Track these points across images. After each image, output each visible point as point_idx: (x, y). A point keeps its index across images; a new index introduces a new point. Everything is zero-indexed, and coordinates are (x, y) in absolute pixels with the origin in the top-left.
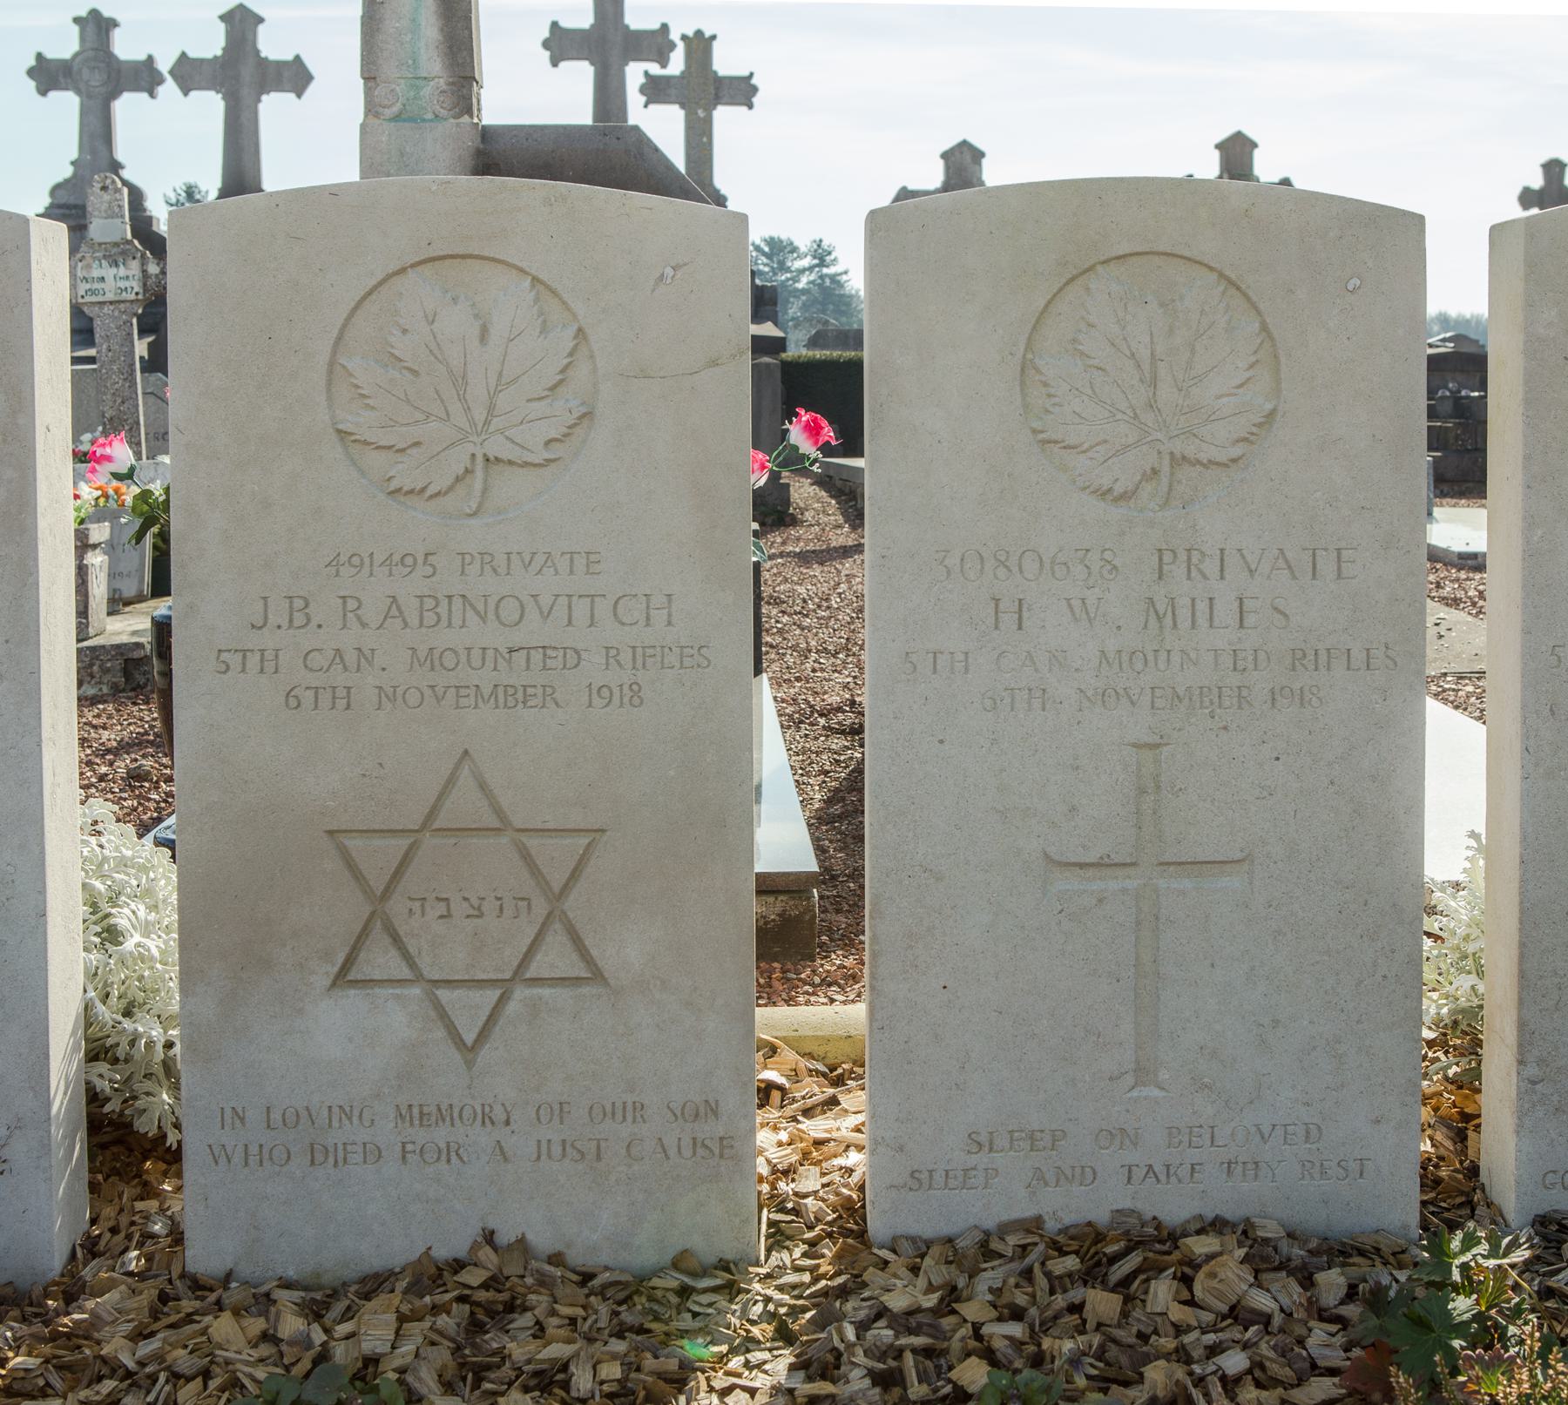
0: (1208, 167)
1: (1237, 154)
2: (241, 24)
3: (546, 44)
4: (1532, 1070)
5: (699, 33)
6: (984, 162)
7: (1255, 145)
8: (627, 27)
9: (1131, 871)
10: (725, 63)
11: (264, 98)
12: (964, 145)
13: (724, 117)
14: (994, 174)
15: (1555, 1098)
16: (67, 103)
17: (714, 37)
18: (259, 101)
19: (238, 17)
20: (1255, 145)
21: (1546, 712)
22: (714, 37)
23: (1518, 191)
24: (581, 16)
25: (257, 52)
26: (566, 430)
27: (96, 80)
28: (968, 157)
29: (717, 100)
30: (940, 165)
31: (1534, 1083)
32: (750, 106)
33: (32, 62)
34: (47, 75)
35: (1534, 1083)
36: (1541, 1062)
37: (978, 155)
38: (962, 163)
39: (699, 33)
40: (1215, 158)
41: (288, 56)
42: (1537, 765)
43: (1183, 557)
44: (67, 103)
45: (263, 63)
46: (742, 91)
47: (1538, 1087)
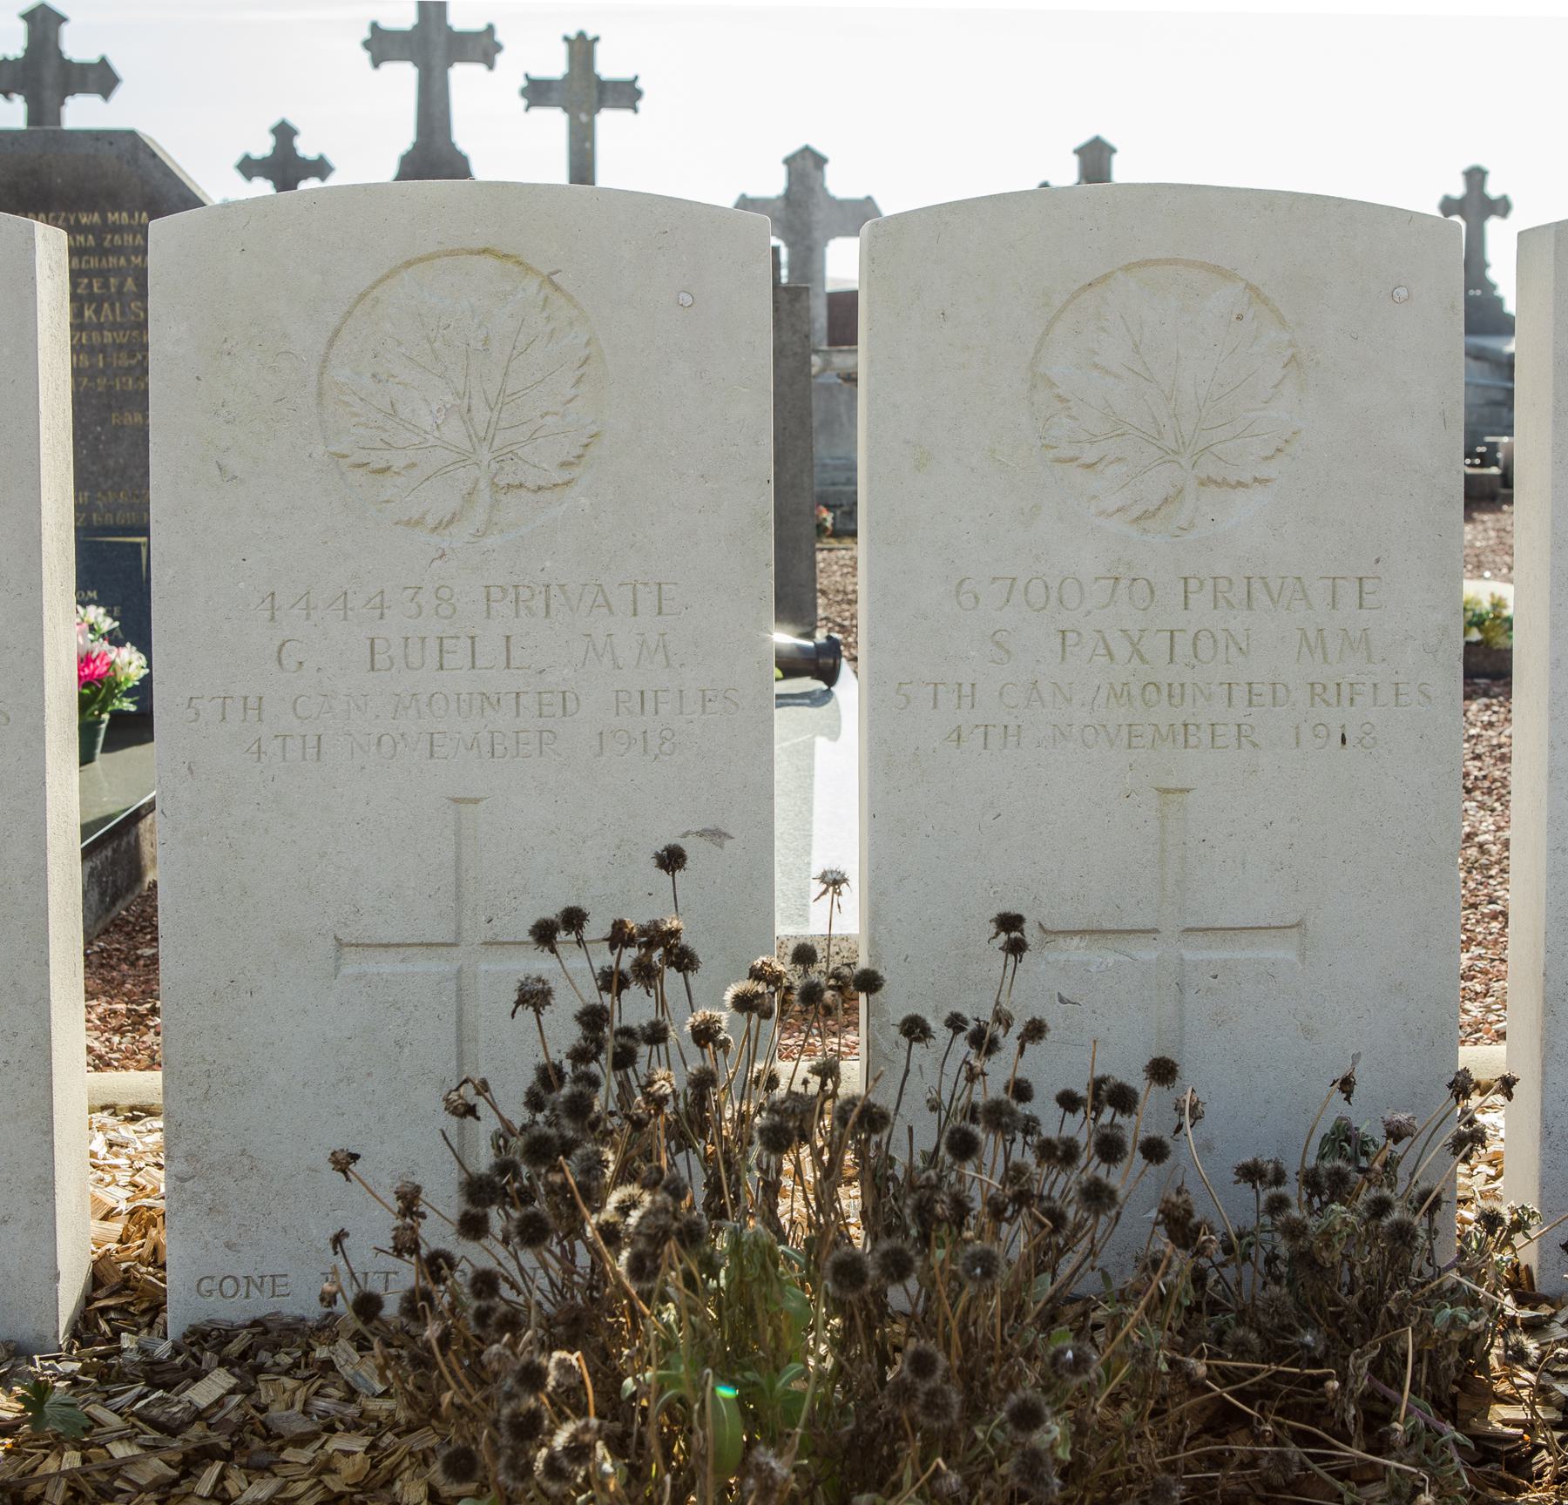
0: (1066, 173)
1: (1095, 159)
2: (43, 24)
3: (367, 45)
4: (180, 1167)
5: (581, 35)
6: (828, 169)
7: (1113, 151)
8: (450, 28)
9: (454, 951)
10: (608, 66)
11: (69, 100)
12: (807, 152)
13: (609, 122)
14: (1123, 171)
15: (209, 1196)
16: (403, 76)
17: (596, 39)
18: (62, 103)
19: (39, 16)
20: (1113, 151)
21: (184, 770)
22: (596, 39)
23: (1485, 165)
24: (402, 15)
25: (60, 53)
26: (579, 451)
27: (49, 74)
28: (810, 163)
29: (601, 103)
30: (782, 171)
31: (183, 1180)
32: (636, 110)
33: (367, 34)
34: (382, 45)
35: (183, 1180)
36: (190, 1157)
37: (820, 161)
38: (1095, 159)
39: (581, 35)
40: (1073, 164)
41: (93, 58)
42: (175, 829)
43: (1209, 584)
44: (403, 76)
45: (67, 65)
46: (626, 94)
47: (187, 1184)
